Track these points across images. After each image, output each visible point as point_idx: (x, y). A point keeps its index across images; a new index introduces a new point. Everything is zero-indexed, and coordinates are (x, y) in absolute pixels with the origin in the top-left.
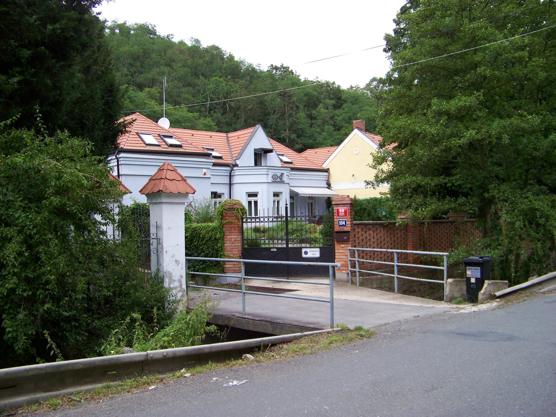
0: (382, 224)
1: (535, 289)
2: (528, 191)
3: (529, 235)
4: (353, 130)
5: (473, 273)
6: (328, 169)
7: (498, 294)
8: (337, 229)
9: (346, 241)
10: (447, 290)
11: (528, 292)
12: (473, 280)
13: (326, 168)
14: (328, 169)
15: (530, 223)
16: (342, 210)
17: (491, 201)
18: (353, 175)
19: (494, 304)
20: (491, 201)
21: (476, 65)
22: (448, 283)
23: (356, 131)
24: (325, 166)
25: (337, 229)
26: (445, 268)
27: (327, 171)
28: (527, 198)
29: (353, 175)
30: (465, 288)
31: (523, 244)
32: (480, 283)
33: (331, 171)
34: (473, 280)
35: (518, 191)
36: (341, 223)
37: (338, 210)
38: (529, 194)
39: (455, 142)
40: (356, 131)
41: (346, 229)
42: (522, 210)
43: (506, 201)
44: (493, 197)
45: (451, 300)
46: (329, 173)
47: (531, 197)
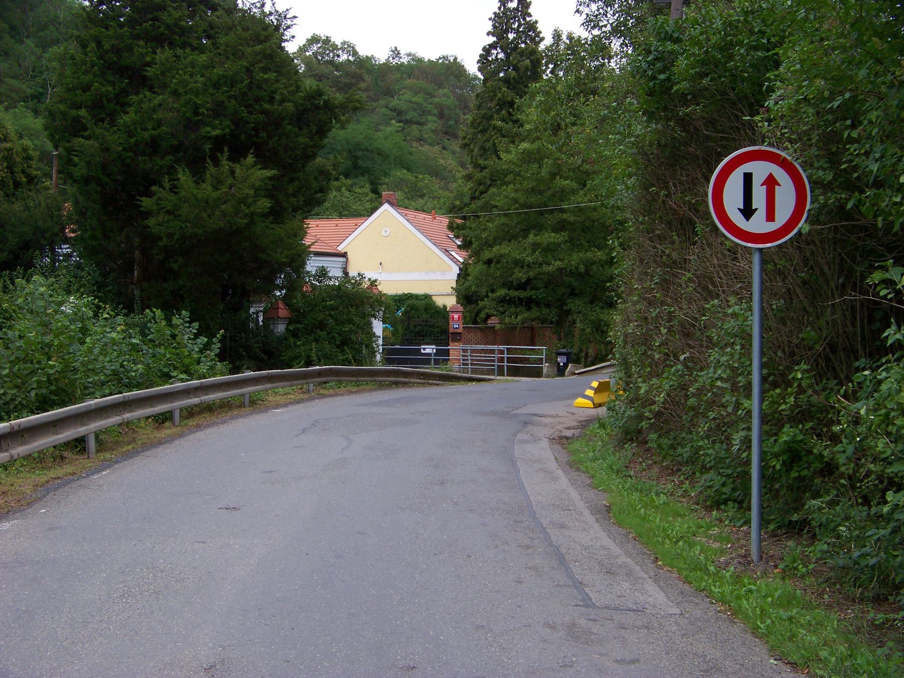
0: (480, 328)
1: (598, 371)
2: (597, 306)
3: (595, 339)
4: (381, 204)
5: (561, 360)
6: (346, 253)
7: (576, 372)
8: (451, 330)
9: (459, 341)
10: (545, 371)
11: (592, 373)
12: (562, 364)
13: (343, 251)
14: (346, 253)
15: (597, 330)
16: (456, 316)
17: (569, 312)
18: (381, 264)
19: (575, 377)
20: (569, 312)
21: (563, 211)
22: (545, 366)
23: (386, 206)
24: (341, 248)
25: (451, 330)
26: (544, 357)
27: (344, 255)
28: (595, 311)
29: (381, 264)
30: (556, 369)
31: (592, 345)
32: (566, 365)
33: (349, 256)
34: (562, 364)
35: (589, 306)
36: (455, 326)
37: (453, 317)
38: (597, 308)
39: (546, 269)
40: (386, 206)
41: (458, 331)
42: (592, 320)
43: (580, 313)
44: (570, 310)
45: (548, 376)
46: (347, 259)
47: (598, 311)
